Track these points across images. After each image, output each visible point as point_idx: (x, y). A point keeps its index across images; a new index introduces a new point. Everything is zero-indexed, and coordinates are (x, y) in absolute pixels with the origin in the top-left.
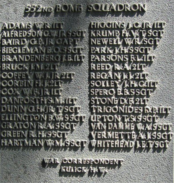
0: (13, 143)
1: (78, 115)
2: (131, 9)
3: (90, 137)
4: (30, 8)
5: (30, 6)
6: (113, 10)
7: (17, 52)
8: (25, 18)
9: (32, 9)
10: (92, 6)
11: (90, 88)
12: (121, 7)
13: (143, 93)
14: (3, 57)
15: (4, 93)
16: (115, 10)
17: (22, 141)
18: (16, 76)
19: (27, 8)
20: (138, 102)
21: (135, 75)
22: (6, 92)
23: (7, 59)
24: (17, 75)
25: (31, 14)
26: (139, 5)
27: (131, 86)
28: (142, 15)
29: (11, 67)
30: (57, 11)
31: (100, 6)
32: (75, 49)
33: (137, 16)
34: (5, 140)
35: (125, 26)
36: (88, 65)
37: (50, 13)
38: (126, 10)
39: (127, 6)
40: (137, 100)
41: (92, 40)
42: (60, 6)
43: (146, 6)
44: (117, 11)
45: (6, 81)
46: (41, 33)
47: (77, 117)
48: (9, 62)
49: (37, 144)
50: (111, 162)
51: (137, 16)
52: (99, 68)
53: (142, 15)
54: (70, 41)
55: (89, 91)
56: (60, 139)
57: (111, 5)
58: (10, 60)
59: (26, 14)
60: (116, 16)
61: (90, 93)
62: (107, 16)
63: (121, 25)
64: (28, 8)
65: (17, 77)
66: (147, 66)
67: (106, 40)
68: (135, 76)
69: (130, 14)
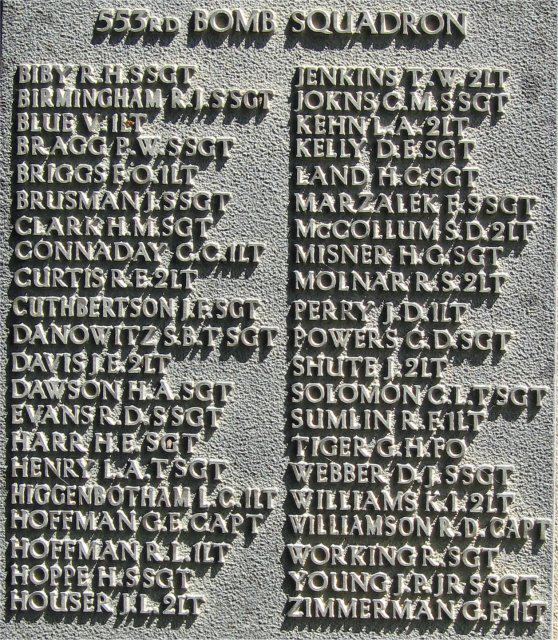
0: (50, 444)
1: (253, 327)
2: (419, 26)
3: (291, 480)
4: (111, 21)
5: (113, 13)
6: (367, 30)
7: (63, 501)
8: (99, 48)
9: (120, 24)
10: (305, 16)
11: (290, 405)
12: (391, 20)
13: (448, 153)
14: (19, 195)
15: (24, 254)
16: (374, 31)
17: (77, 274)
18: (58, 553)
19: (102, 17)
20: (435, 127)
21: (426, 125)
22: (31, 252)
23: (32, 204)
24: (61, 520)
25: (115, 38)
26: (445, 17)
27: (409, 455)
28: (455, 45)
29: (45, 202)
30: (198, 29)
31: (329, 16)
32: (250, 335)
33: (441, 47)
34: (23, 539)
35: (397, 343)
36: (287, 198)
37: (172, 35)
38: (406, 32)
39: (410, 18)
40: (433, 122)
41: (299, 274)
42: (207, 14)
43: (466, 22)
44: (381, 36)
45: (30, 244)
46: (139, 548)
47: (250, 335)
48: (40, 158)
49: (120, 557)
50: (346, 450)
51: (441, 47)
52: (320, 151)
53: (455, 45)
54: (235, 524)
55: (288, 415)
56: (201, 481)
57: (362, 15)
58: (45, 151)
59: (97, 38)
60: (376, 47)
61: (293, 368)
62: (350, 47)
63: (386, 78)
64: (106, 19)
65: (61, 580)
66: (454, 278)
67: (345, 333)
68: (427, 128)
69: (415, 40)
